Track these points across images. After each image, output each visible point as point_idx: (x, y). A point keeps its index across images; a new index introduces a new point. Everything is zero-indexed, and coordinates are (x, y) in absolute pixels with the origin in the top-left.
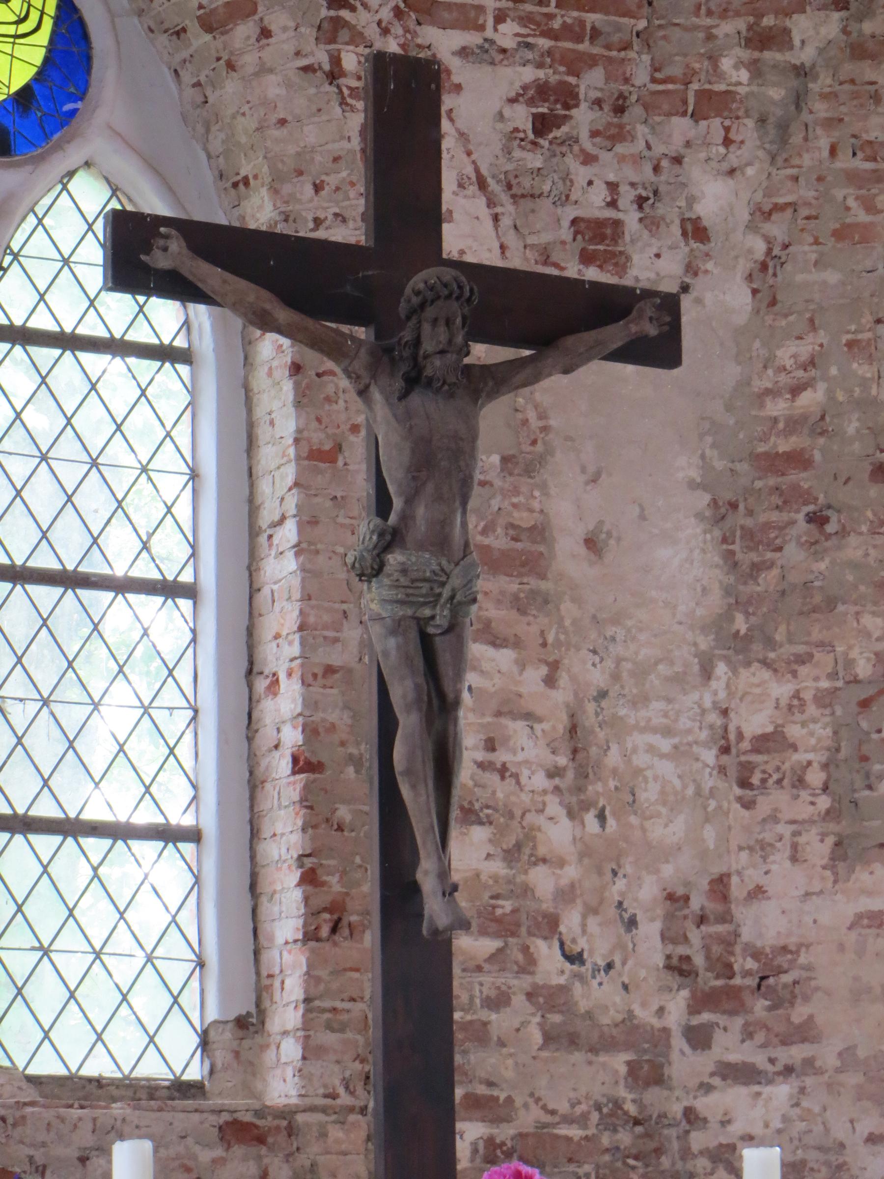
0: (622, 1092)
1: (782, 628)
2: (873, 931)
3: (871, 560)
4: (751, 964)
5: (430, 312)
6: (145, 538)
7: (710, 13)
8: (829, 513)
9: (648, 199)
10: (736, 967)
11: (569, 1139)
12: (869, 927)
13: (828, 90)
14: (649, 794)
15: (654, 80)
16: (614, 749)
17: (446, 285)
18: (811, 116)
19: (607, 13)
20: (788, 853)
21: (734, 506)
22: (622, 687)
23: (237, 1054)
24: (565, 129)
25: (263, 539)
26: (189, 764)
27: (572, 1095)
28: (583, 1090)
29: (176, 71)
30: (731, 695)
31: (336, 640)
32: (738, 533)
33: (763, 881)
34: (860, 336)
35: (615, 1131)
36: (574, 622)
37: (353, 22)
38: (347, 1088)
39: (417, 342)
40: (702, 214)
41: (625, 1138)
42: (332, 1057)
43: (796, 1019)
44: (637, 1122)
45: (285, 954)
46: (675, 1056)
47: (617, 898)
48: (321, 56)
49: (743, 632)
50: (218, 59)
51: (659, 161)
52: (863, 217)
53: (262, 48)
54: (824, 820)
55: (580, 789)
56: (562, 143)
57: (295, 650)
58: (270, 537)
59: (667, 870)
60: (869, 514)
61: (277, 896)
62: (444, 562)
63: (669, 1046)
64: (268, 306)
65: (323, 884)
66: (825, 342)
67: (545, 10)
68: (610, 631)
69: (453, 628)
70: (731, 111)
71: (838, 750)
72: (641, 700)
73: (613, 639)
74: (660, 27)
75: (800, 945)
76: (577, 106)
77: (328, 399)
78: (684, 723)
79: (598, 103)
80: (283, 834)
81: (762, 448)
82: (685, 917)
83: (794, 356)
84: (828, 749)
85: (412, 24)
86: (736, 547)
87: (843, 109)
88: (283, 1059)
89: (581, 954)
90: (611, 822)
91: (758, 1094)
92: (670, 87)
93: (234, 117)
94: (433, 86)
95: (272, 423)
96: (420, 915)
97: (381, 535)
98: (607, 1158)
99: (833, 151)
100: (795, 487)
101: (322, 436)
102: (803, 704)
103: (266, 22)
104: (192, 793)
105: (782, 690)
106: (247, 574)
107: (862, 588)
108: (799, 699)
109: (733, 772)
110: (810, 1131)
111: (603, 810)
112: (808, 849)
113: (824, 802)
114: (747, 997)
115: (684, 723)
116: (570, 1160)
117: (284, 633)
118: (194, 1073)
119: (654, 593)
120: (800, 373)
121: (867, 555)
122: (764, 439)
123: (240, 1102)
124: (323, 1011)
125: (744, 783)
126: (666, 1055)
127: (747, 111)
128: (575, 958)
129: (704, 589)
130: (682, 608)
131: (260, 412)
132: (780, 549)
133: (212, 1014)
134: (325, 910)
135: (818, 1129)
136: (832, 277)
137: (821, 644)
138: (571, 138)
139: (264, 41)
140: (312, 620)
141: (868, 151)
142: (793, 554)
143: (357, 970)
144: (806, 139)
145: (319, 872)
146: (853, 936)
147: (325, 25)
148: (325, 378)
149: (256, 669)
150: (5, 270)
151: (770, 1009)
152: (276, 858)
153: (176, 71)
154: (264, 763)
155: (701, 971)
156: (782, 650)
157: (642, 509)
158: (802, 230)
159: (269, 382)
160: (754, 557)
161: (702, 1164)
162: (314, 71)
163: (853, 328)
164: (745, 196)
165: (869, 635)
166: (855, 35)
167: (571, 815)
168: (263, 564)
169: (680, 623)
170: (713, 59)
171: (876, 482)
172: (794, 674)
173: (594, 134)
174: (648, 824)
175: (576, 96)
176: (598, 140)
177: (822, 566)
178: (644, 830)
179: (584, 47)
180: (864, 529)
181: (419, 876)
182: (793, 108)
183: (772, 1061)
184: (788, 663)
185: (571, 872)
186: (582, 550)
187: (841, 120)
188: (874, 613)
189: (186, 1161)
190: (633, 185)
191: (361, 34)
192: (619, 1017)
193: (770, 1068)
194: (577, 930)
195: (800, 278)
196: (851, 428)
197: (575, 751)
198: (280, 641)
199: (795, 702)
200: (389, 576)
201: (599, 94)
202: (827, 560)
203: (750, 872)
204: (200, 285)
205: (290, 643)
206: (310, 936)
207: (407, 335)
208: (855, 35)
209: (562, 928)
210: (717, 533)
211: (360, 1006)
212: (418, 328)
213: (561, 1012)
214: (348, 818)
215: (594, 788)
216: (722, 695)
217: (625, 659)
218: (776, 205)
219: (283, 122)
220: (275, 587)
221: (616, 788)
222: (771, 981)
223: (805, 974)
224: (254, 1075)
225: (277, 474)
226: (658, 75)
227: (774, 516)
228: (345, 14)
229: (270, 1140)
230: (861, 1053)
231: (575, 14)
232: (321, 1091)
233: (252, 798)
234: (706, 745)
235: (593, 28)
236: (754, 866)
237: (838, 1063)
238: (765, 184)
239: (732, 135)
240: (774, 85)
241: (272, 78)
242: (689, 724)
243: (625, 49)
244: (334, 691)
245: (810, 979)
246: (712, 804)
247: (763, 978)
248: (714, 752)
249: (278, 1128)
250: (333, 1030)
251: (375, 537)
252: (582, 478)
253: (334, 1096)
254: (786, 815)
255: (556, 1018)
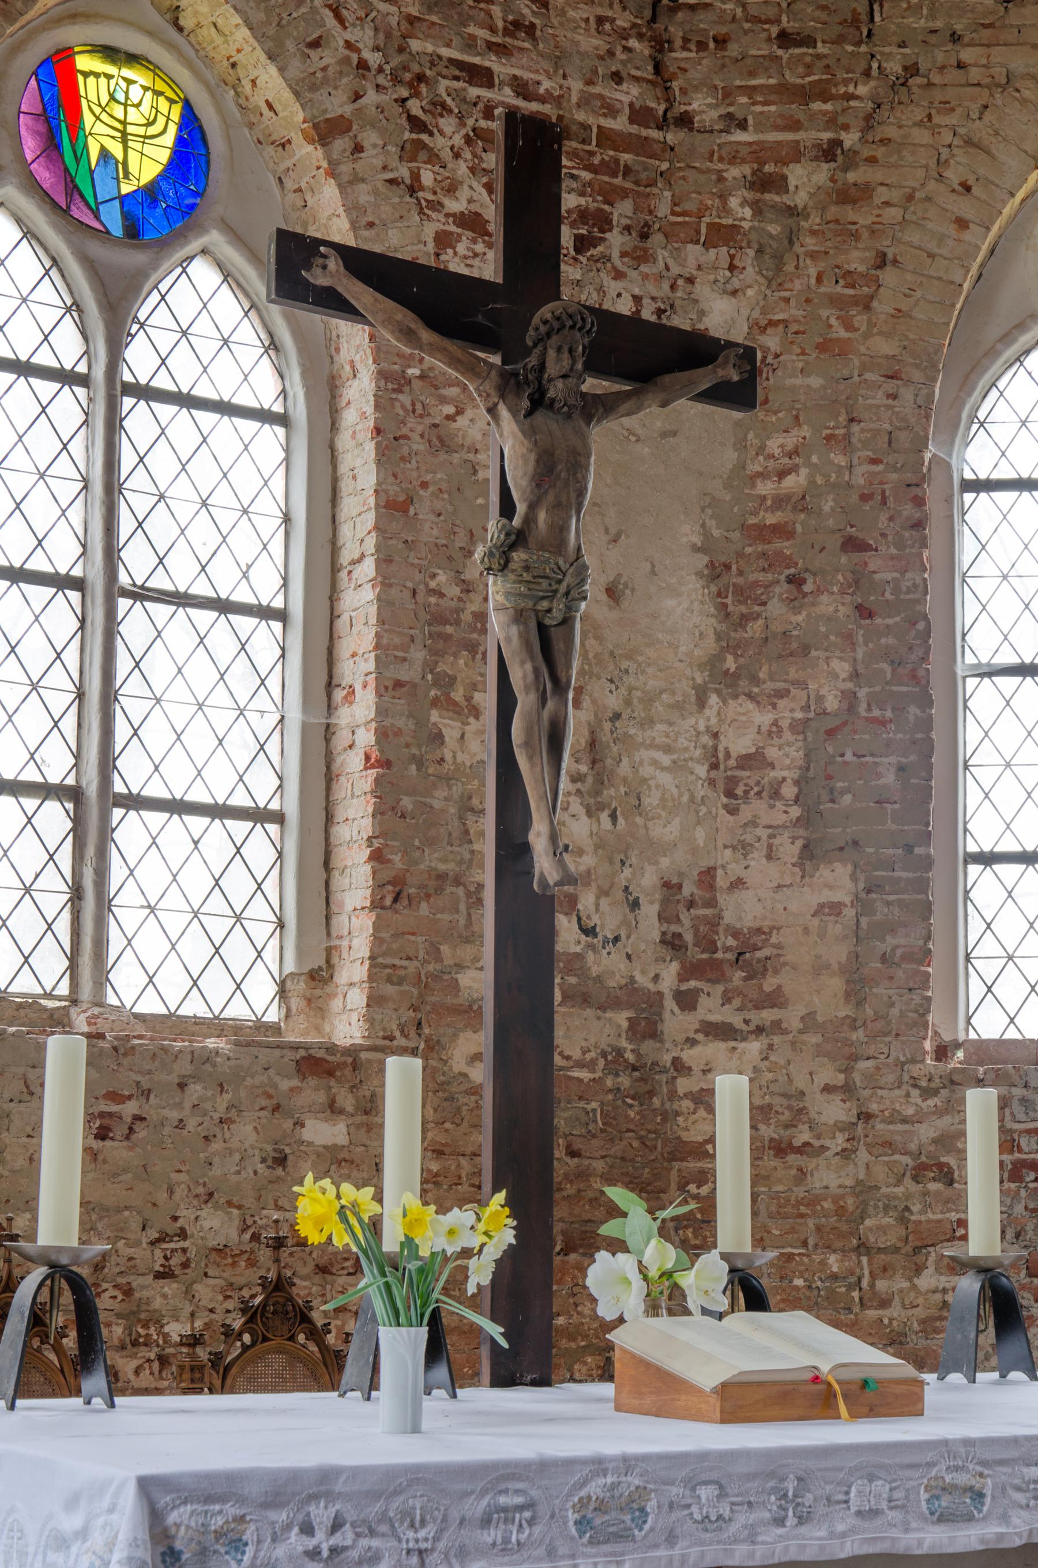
0: (624, 1043)
1: (765, 668)
2: (832, 918)
3: (840, 614)
4: (731, 942)
5: (555, 340)
6: (244, 569)
7: (721, 159)
8: (806, 575)
9: (665, 311)
10: (719, 945)
11: (580, 1080)
12: (830, 915)
13: (817, 228)
14: (651, 800)
15: (674, 213)
16: (625, 761)
17: (570, 316)
18: (802, 250)
19: (638, 155)
20: (764, 853)
21: (727, 567)
22: (633, 711)
23: (309, 1001)
24: (600, 249)
25: (343, 574)
26: (276, 759)
27: (584, 1044)
28: (592, 1040)
29: (280, 178)
30: (721, 721)
31: (405, 659)
32: (731, 589)
33: (743, 874)
34: (837, 432)
35: (617, 1075)
36: (596, 656)
37: (432, 145)
38: (402, 1031)
39: (542, 367)
40: (709, 326)
41: (625, 1081)
42: (391, 1005)
43: (767, 989)
44: (635, 1068)
45: (353, 919)
46: (667, 1015)
47: (624, 883)
48: (403, 172)
49: (732, 670)
50: (318, 168)
51: (676, 280)
52: (843, 334)
53: (355, 161)
54: (795, 826)
55: (597, 793)
56: (597, 261)
57: (371, 666)
58: (350, 572)
59: (665, 862)
60: (840, 577)
61: (348, 870)
62: (561, 563)
63: (662, 1006)
64: (413, 326)
65: (389, 861)
66: (808, 435)
67: (587, 148)
68: (624, 665)
69: (567, 621)
70: (735, 241)
71: (808, 769)
72: (648, 722)
73: (627, 671)
74: (680, 168)
75: (772, 928)
76: (610, 230)
77: (403, 459)
78: (682, 742)
79: (628, 228)
80: (354, 819)
81: (752, 521)
82: (678, 901)
83: (782, 446)
84: (800, 768)
85: (479, 150)
86: (729, 601)
87: (829, 244)
88: (349, 1007)
89: (594, 928)
90: (621, 821)
91: (734, 1049)
92: (687, 219)
93: (329, 218)
94: (556, 146)
95: (354, 478)
96: (529, 873)
97: (508, 535)
98: (610, 1097)
99: (819, 279)
100: (779, 554)
101: (397, 489)
102: (780, 730)
103: (359, 139)
104: (278, 782)
105: (764, 718)
106: (328, 603)
107: (832, 638)
108: (777, 726)
109: (721, 785)
110: (777, 1080)
111: (615, 809)
112: (782, 849)
113: (795, 812)
114: (726, 967)
115: (682, 742)
116: (580, 1098)
117: (361, 652)
118: (273, 1016)
119: (660, 636)
120: (786, 460)
121: (837, 611)
122: (754, 513)
123: (312, 1039)
124: (386, 966)
125: (730, 794)
126: (660, 1014)
127: (749, 243)
128: (589, 931)
129: (701, 634)
130: (683, 649)
131: (343, 469)
132: (764, 604)
133: (290, 967)
134: (389, 883)
135: (782, 1078)
136: (815, 382)
137: (796, 683)
138: (604, 257)
139: (356, 155)
140: (385, 641)
141: (849, 280)
142: (775, 608)
143: (414, 934)
144: (797, 267)
145: (384, 852)
146: (816, 922)
147: (408, 146)
148: (401, 441)
149: (335, 682)
150: (133, 336)
151: (746, 979)
152: (348, 838)
153: (280, 178)
154: (339, 760)
155: (690, 946)
156: (764, 686)
157: (653, 566)
158: (792, 343)
159: (354, 443)
160: (743, 609)
161: (687, 1104)
162: (398, 184)
163: (832, 424)
164: (745, 313)
165: (836, 676)
166: (840, 183)
167: (589, 813)
168: (343, 595)
169: (681, 661)
170: (723, 197)
171: (846, 552)
172: (774, 706)
173: (623, 255)
174: (650, 824)
175: (609, 222)
176: (626, 260)
177: (800, 618)
178: (647, 829)
179: (618, 181)
180: (835, 589)
181: (531, 837)
182: (786, 242)
183: (746, 1022)
184: (769, 696)
185: (588, 861)
186: (604, 597)
187: (826, 253)
188: (841, 659)
189: (268, 1089)
190: (653, 299)
191: (437, 155)
192: (623, 982)
193: (744, 1027)
194: (592, 908)
195: (789, 382)
196: (827, 506)
197: (594, 762)
198: (357, 658)
199: (774, 729)
200: (513, 571)
201: (628, 222)
202: (804, 613)
203: (733, 866)
204: (353, 302)
205: (366, 661)
206: (376, 904)
207: (533, 361)
208: (840, 183)
209: (580, 906)
210: (714, 589)
211: (416, 963)
212: (544, 353)
213: (576, 975)
214: (410, 807)
215: (609, 793)
216: (714, 721)
217: (636, 689)
218: (770, 321)
219: (371, 225)
220: (353, 614)
221: (626, 793)
222: (748, 955)
223: (775, 952)
224: (323, 1019)
225: (358, 520)
226: (677, 209)
227: (761, 576)
228: (424, 137)
229: (338, 1073)
230: (820, 1019)
231: (611, 153)
232: (381, 1034)
233: (328, 789)
234: (698, 761)
235: (626, 166)
236: (736, 862)
237: (801, 1026)
238: (762, 303)
239: (737, 262)
240: (771, 222)
241: (363, 186)
242: (686, 744)
243: (650, 186)
244: (402, 701)
245: (779, 955)
246: (703, 810)
247: (740, 954)
248: (706, 767)
249: (345, 1063)
250: (392, 983)
251: (502, 536)
252: (605, 538)
253: (391, 1038)
254: (764, 821)
255: (573, 980)
